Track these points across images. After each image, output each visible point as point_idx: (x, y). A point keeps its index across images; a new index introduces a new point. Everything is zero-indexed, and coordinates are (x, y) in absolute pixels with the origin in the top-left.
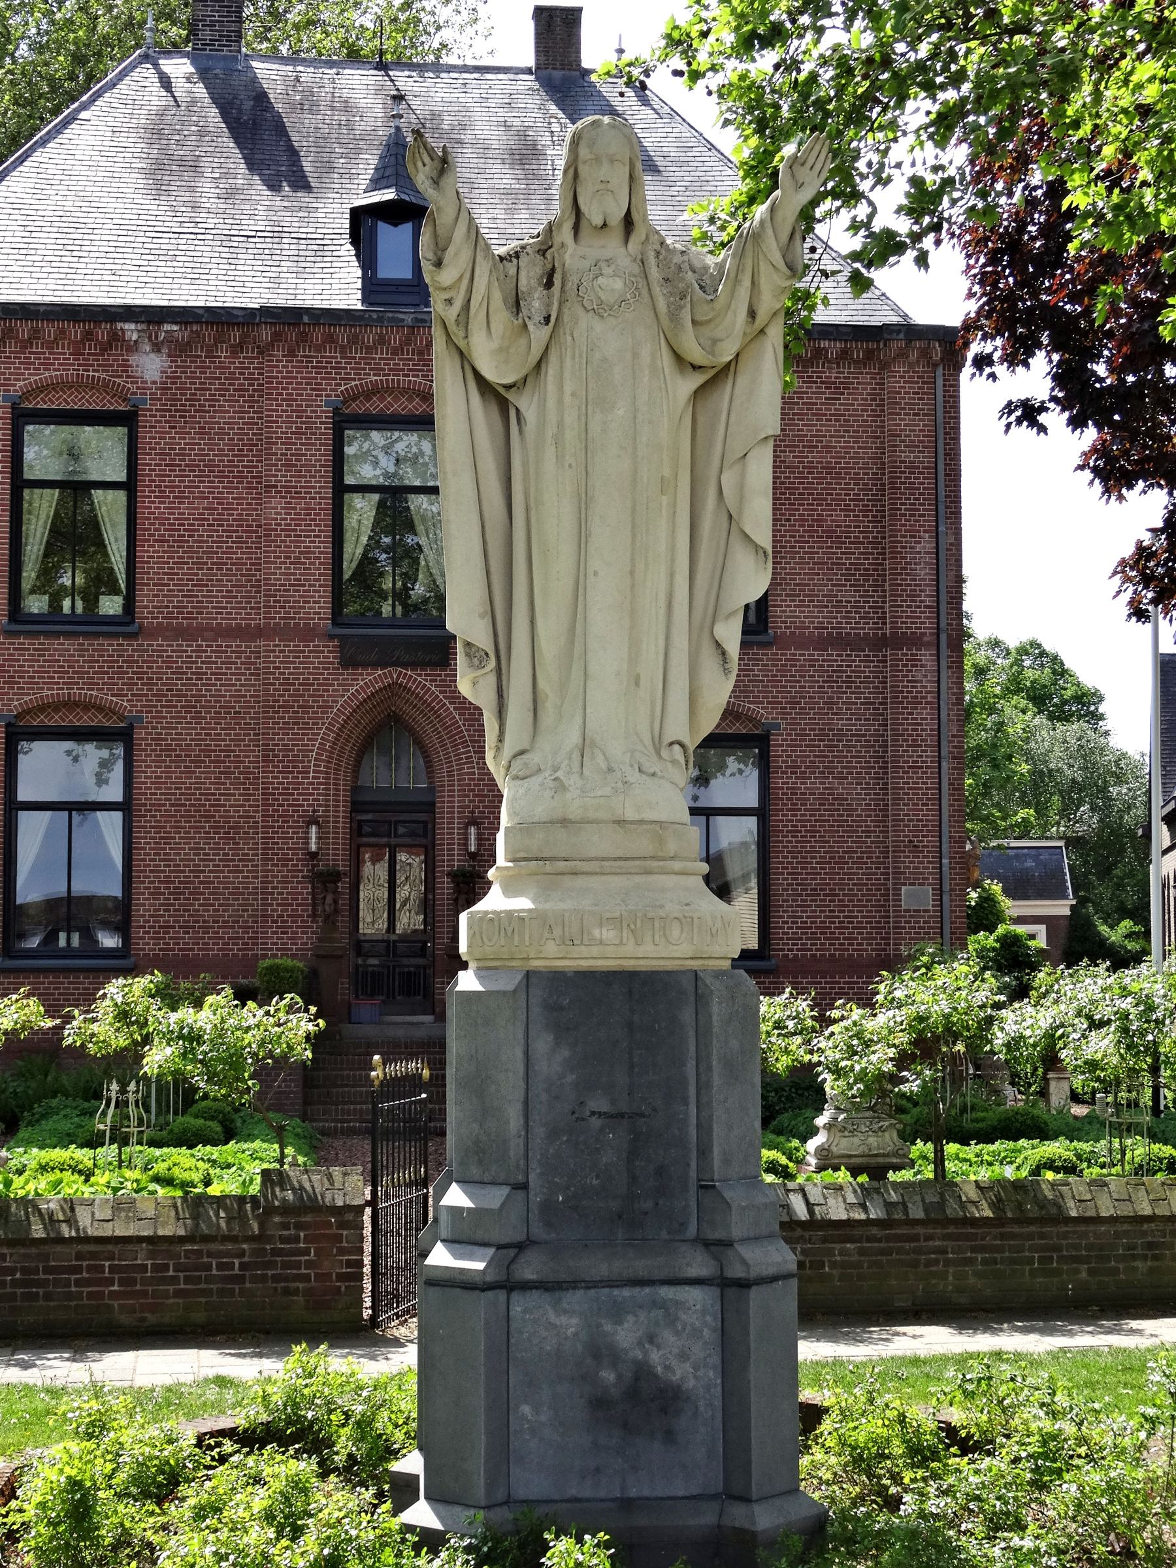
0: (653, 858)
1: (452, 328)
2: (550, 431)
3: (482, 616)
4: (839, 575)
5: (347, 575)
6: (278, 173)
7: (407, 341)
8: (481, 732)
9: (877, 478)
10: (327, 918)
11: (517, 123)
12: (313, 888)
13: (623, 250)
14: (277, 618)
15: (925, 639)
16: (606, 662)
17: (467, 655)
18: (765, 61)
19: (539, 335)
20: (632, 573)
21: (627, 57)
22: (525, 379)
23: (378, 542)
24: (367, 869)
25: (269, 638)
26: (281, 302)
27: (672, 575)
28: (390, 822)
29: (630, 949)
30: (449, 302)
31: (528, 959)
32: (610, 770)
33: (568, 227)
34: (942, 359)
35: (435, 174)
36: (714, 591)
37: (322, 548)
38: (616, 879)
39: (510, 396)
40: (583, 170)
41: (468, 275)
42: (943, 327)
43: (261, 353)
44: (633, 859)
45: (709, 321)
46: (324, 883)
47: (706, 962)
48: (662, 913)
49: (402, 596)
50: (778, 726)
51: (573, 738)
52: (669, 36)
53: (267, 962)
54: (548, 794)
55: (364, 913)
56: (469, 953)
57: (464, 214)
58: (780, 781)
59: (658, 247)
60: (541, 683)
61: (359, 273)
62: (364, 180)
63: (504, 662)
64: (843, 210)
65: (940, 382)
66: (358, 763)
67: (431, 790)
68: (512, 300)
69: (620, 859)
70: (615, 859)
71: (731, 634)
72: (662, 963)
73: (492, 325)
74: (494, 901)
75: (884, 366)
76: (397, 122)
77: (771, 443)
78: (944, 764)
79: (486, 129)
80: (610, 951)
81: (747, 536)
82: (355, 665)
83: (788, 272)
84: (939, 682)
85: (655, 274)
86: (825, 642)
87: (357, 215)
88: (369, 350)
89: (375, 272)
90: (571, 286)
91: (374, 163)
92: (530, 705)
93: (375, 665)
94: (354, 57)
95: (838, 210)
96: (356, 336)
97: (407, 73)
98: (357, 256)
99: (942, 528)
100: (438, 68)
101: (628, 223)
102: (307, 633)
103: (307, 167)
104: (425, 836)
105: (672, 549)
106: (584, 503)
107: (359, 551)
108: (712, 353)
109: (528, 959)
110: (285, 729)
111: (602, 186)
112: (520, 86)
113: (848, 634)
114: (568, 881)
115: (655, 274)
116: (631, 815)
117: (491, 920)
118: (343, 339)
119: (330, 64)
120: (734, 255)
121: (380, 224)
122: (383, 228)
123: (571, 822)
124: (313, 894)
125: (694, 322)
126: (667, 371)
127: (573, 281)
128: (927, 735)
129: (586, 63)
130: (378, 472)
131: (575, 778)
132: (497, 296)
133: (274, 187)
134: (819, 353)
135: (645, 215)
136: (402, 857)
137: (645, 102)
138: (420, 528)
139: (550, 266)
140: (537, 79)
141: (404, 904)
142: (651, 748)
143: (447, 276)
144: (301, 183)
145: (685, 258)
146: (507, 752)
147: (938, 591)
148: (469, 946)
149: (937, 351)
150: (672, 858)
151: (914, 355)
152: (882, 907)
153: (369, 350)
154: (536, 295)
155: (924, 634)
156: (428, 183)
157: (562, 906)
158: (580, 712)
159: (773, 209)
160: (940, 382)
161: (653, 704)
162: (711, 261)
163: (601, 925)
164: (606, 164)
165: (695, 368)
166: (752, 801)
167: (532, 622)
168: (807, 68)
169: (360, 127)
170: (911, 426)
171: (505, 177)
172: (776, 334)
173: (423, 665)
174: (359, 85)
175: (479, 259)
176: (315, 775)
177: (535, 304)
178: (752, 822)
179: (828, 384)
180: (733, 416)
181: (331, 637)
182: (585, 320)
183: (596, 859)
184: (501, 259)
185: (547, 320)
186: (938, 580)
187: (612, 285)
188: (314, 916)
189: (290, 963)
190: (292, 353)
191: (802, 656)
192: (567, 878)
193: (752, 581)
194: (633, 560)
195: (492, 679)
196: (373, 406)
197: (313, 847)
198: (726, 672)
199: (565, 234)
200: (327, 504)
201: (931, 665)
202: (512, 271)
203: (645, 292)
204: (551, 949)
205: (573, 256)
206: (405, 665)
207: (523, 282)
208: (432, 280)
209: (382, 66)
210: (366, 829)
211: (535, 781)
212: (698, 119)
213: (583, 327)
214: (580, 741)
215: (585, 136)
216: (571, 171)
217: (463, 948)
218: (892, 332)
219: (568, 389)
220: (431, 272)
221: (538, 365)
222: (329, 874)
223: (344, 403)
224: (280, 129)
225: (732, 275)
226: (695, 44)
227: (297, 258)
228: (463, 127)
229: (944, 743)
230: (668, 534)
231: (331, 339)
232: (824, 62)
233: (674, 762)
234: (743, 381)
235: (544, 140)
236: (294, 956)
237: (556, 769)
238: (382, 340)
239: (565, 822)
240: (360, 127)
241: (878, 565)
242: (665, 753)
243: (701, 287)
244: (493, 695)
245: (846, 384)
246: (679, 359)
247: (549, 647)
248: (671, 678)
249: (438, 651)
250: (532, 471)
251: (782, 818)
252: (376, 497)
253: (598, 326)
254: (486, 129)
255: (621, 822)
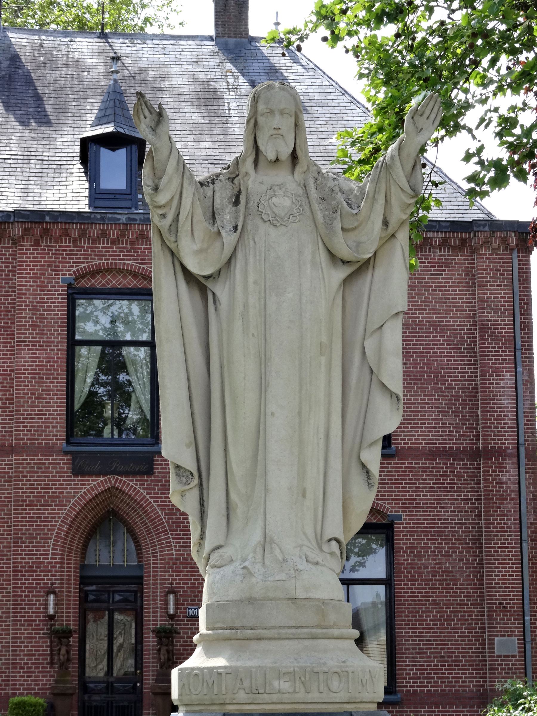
0: (317, 626)
1: (166, 235)
2: (239, 308)
3: (188, 446)
4: (443, 404)
5: (77, 406)
6: (27, 113)
7: (122, 234)
8: (187, 531)
9: (471, 332)
10: (62, 665)
11: (202, 76)
12: (51, 642)
13: (290, 177)
14: (25, 438)
15: (509, 451)
16: (280, 479)
17: (178, 475)
18: (388, 31)
19: (229, 239)
20: (300, 414)
21: (282, 29)
22: (219, 272)
23: (98, 380)
24: (91, 627)
25: (19, 454)
26: (29, 207)
27: (328, 415)
28: (109, 592)
29: (301, 696)
30: (164, 216)
31: (224, 704)
32: (285, 560)
33: (250, 160)
34: (517, 245)
35: (153, 124)
36: (361, 425)
37: (59, 388)
38: (290, 642)
39: (209, 284)
40: (261, 120)
41: (177, 197)
42: (517, 222)
43: (14, 243)
44: (302, 627)
45: (354, 229)
46: (59, 638)
47: (358, 706)
48: (326, 669)
49: (119, 422)
50: (399, 517)
51: (257, 536)
52: (318, 14)
53: (16, 699)
54: (238, 579)
55: (89, 661)
56: (180, 700)
57: (174, 152)
58: (400, 558)
59: (316, 175)
60: (233, 496)
61: (87, 185)
62: (90, 118)
63: (204, 484)
64: (447, 138)
65: (515, 262)
66: (85, 547)
67: (140, 567)
68: (210, 214)
69: (293, 627)
70: (289, 628)
71: (373, 458)
72: (325, 706)
73: (196, 234)
74: (197, 660)
75: (474, 251)
76: (115, 76)
77: (400, 318)
78: (525, 545)
79: (180, 80)
80: (286, 697)
81: (384, 386)
82: (83, 474)
83: (412, 193)
84: (519, 483)
85: (314, 194)
86: (434, 454)
87: (85, 143)
88: (94, 241)
89: (98, 184)
90: (253, 204)
91: (97, 105)
92: (224, 512)
93: (98, 474)
94: (83, 28)
95: (442, 138)
96: (84, 230)
97: (121, 40)
98: (86, 172)
99: (519, 369)
100: (144, 37)
101: (294, 157)
102: (48, 450)
103: (49, 108)
104: (136, 601)
105: (329, 395)
106: (264, 362)
107: (86, 390)
108: (358, 252)
109: (224, 704)
110: (31, 523)
111: (276, 132)
112: (205, 49)
113: (451, 448)
114: (254, 645)
115: (314, 194)
116: (301, 594)
117: (197, 675)
118: (75, 232)
119: (65, 33)
120: (372, 181)
121: (102, 149)
122: (104, 152)
123: (256, 600)
124: (51, 646)
125: (343, 230)
126: (324, 264)
127: (254, 200)
128: (512, 524)
129: (253, 32)
130: (98, 327)
131: (259, 566)
132: (199, 211)
133: (24, 123)
134: (426, 241)
135: (307, 152)
136: (118, 617)
137: (296, 60)
138: (131, 368)
139: (237, 189)
140: (217, 44)
141: (119, 651)
142: (315, 544)
143: (162, 198)
144: (44, 120)
145: (336, 183)
146: (207, 547)
147: (517, 416)
148: (180, 695)
149: (513, 240)
150: (332, 627)
151: (496, 243)
152: (481, 653)
153: (94, 241)
154: (227, 211)
155: (509, 448)
156: (148, 130)
157: (249, 663)
158: (261, 517)
159: (400, 148)
160: (515, 262)
161: (316, 509)
162: (354, 185)
163: (279, 678)
164: (277, 116)
165: (345, 262)
166: (380, 572)
167: (226, 450)
168: (420, 36)
169: (88, 79)
170: (494, 295)
171: (193, 115)
172: (403, 236)
173: (134, 473)
174: (85, 48)
175: (185, 185)
176: (52, 559)
177: (227, 217)
178: (381, 589)
179: (433, 264)
180: (372, 299)
181: (66, 453)
182: (263, 228)
183: (275, 628)
184: (202, 184)
185: (236, 228)
186: (517, 408)
187: (283, 203)
188: (52, 663)
189: (33, 699)
190: (37, 244)
191: (418, 464)
192: (253, 642)
193: (388, 419)
194: (300, 404)
195: (196, 492)
196: (98, 282)
197: (51, 611)
198: (370, 486)
199: (248, 165)
200: (63, 354)
201: (513, 471)
202: (210, 193)
203: (307, 208)
204: (242, 696)
205: (255, 182)
206: (120, 474)
207: (217, 201)
208: (152, 201)
209: (103, 36)
210: (91, 597)
211: (228, 570)
212: (339, 77)
213: (263, 234)
214: (262, 539)
215: (263, 96)
216: (252, 121)
217: (175, 695)
218: (479, 226)
219: (251, 279)
220: (149, 195)
221: (229, 261)
222: (64, 632)
223: (75, 280)
224: (29, 82)
225: (371, 195)
226: (337, 18)
227: (41, 175)
228: (163, 79)
229: (524, 529)
230: (325, 383)
231: (66, 233)
232: (432, 32)
233: (332, 554)
234: (379, 272)
235: (222, 88)
236: (36, 695)
237: (244, 560)
238: (104, 234)
239: (251, 600)
240: (88, 79)
241: (473, 397)
242: (325, 548)
243: (348, 204)
244: (197, 505)
245: (447, 264)
246: (332, 256)
247: (238, 470)
248: (329, 491)
249: (146, 461)
250: (225, 339)
251: (404, 587)
252: (99, 348)
253: (273, 232)
254: (180, 80)
255: (293, 600)
